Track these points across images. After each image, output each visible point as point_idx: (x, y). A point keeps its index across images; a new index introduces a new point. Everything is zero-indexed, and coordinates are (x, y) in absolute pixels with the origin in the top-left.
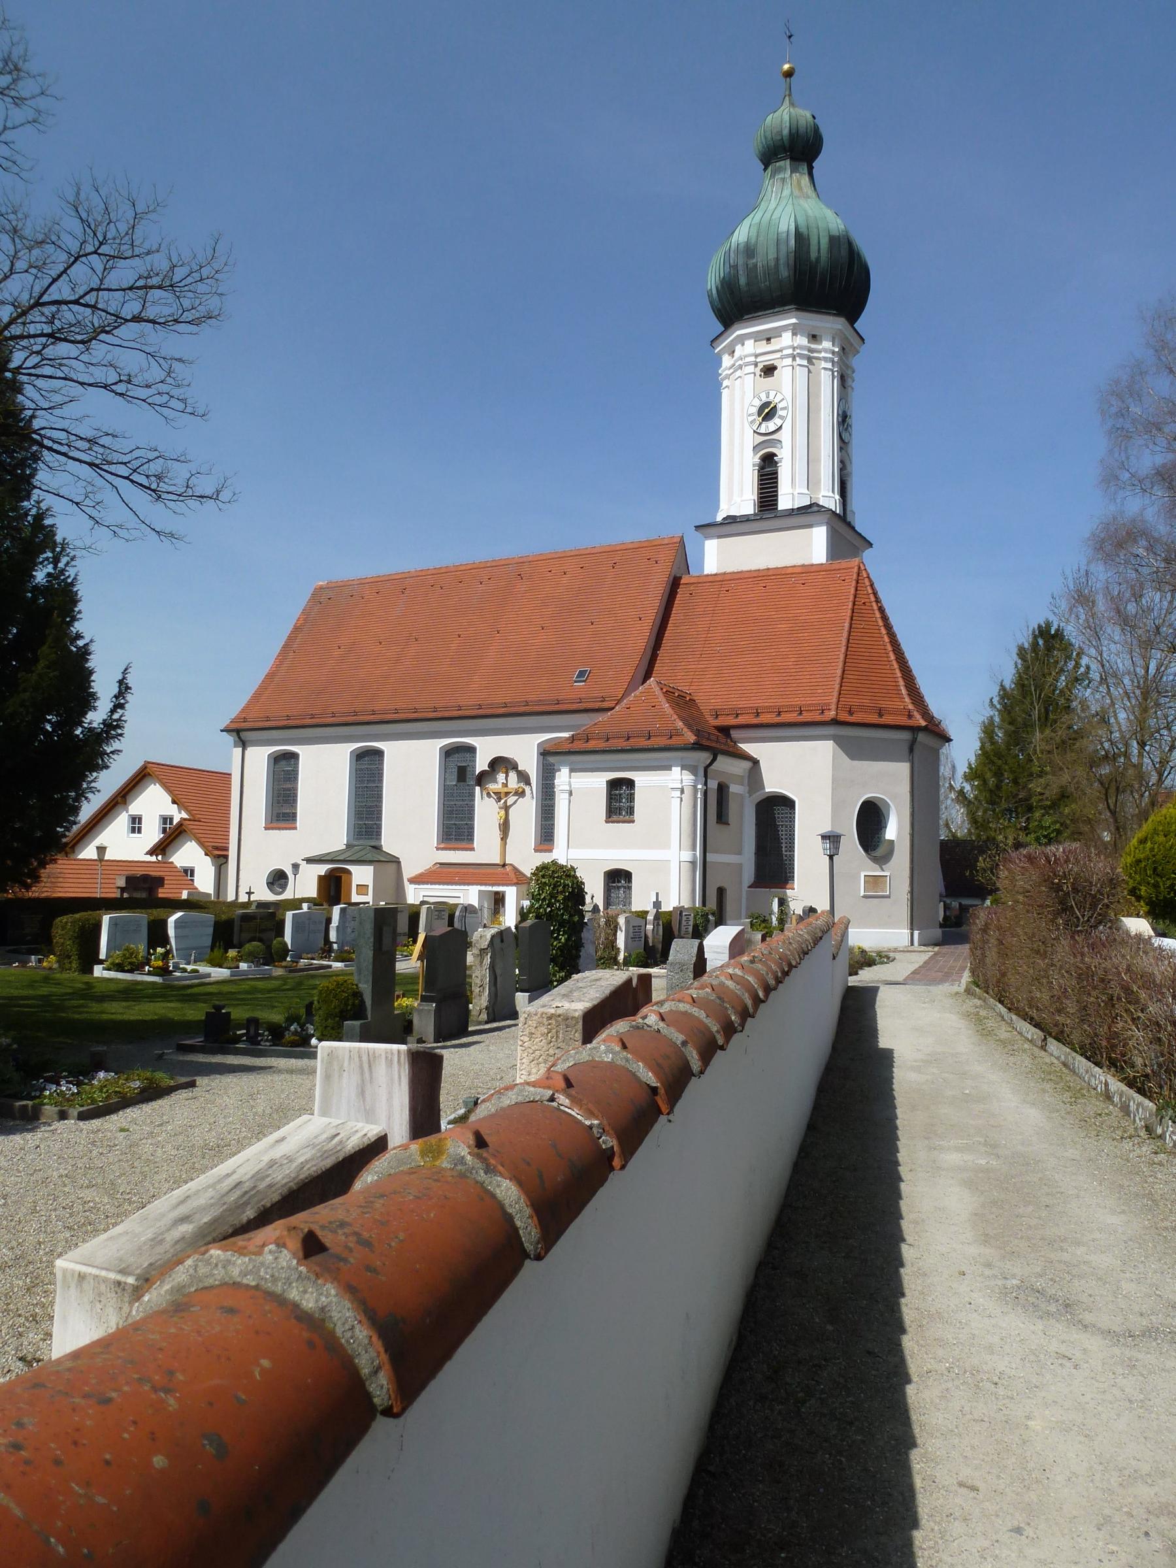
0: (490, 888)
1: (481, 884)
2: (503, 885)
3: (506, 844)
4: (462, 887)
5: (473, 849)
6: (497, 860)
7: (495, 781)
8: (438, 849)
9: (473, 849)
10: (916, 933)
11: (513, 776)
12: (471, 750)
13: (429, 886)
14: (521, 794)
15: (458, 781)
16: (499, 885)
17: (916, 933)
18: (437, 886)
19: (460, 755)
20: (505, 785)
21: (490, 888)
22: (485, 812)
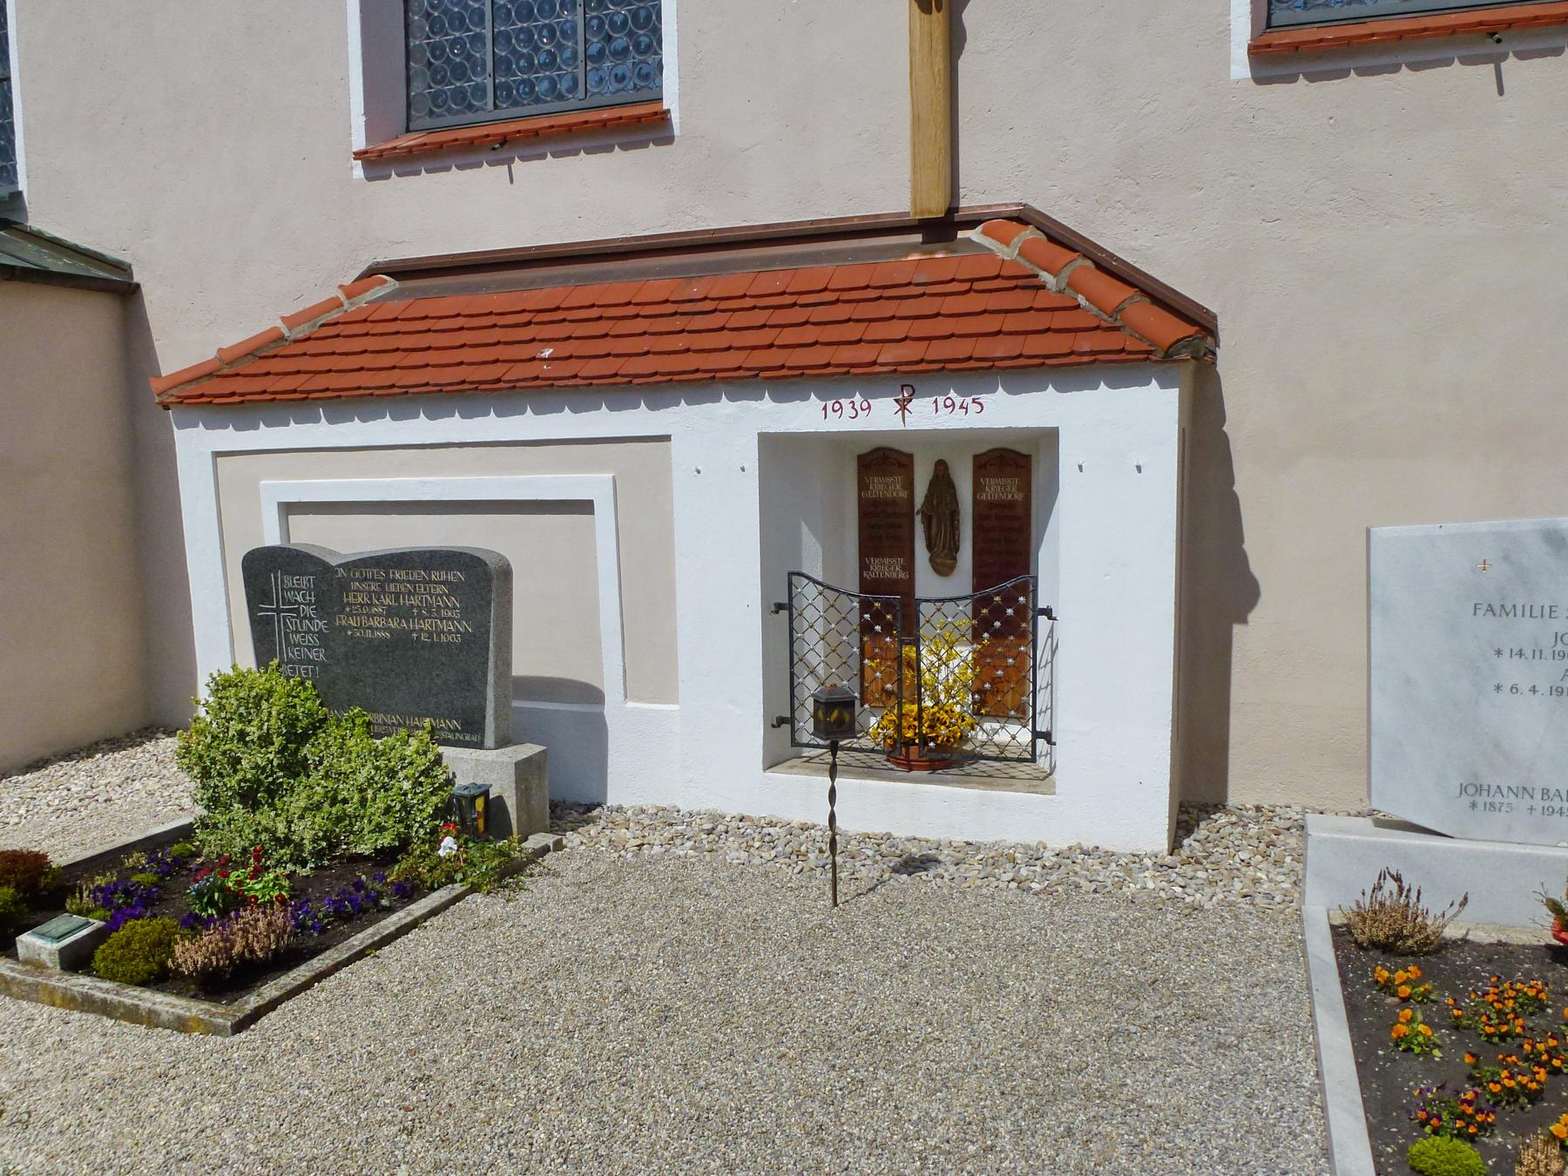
0: (1482, 526)
1: (787, 381)
2: (1025, 371)
3: (955, 40)
5: (649, 126)
6: (891, 193)
21: (1482, 526)
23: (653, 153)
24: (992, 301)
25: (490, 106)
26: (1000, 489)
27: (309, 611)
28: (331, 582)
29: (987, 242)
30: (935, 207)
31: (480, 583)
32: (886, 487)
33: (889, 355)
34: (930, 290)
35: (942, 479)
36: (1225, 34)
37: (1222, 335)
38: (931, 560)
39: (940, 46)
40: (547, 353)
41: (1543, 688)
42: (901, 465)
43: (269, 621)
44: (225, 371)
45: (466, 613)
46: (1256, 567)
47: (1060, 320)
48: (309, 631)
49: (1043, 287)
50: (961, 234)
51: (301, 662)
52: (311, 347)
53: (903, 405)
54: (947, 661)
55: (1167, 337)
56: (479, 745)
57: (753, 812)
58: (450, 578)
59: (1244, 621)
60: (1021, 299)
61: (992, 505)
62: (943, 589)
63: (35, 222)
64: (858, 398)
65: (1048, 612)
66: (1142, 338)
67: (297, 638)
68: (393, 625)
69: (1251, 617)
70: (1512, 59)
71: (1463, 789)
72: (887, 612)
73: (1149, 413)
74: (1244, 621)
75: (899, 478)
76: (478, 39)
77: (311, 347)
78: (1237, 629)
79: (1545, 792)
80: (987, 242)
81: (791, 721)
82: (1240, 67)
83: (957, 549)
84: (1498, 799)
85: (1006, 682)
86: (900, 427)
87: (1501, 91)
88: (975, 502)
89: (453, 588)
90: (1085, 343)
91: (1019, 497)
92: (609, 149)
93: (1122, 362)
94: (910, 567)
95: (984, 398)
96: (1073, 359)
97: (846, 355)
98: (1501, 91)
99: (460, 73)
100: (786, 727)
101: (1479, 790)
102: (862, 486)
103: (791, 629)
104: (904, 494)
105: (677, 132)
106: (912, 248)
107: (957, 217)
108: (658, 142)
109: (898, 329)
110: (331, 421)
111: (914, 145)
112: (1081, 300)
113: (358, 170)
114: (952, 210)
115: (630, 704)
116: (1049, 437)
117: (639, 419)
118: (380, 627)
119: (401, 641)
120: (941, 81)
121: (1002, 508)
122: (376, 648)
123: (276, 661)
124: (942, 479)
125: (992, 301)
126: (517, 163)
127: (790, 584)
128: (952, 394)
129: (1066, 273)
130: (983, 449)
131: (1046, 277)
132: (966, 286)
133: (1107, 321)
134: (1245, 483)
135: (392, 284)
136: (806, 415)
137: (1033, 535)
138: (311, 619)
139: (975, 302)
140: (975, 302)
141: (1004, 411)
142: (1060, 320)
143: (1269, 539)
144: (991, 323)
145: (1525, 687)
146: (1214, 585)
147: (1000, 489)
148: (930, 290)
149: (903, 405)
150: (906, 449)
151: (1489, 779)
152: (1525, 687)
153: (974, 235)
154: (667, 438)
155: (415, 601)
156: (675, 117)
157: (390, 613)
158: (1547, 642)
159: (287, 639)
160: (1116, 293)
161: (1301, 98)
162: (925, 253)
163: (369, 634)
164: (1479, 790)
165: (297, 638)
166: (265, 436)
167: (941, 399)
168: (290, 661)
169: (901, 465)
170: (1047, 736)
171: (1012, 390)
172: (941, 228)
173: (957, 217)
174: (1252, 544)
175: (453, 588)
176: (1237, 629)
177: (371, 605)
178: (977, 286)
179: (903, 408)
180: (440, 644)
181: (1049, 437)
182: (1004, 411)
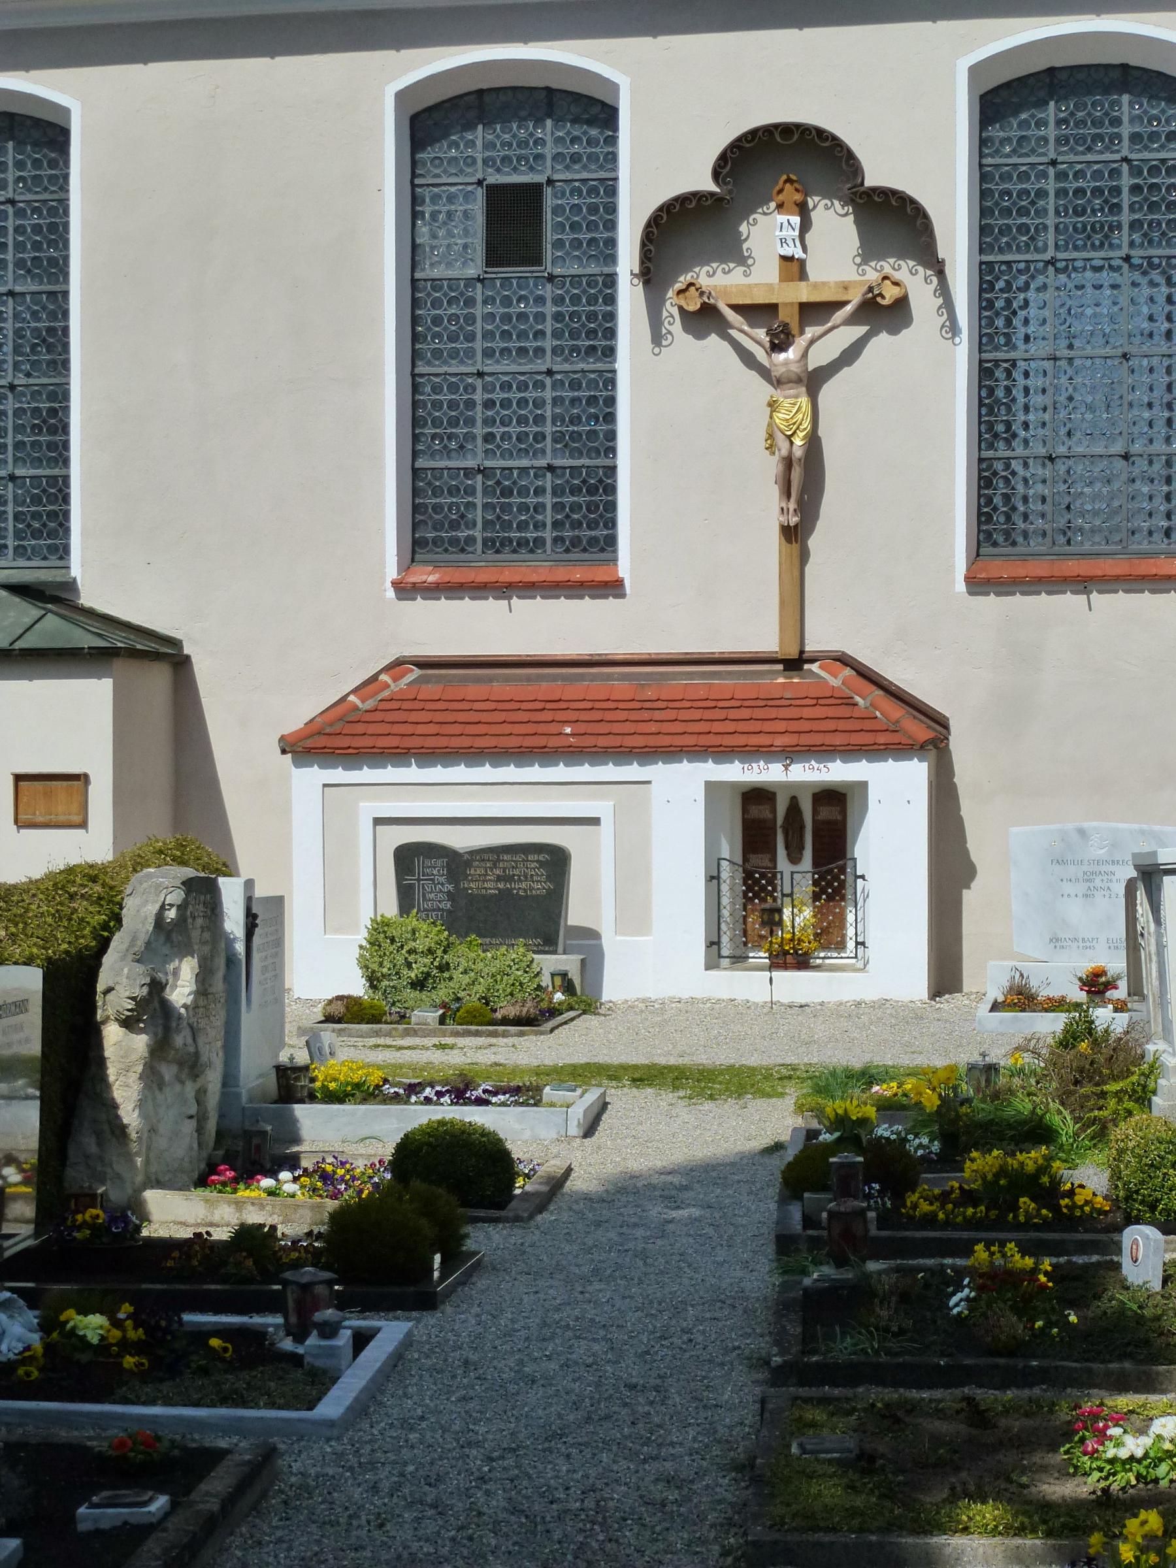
0: (1053, 827)
1: (723, 753)
2: (851, 752)
3: (804, 556)
4: (609, 771)
5: (613, 588)
6: (766, 638)
7: (733, 252)
8: (404, 590)
9: (613, 588)
10: (751, 955)
11: (835, 230)
12: (594, 111)
13: (412, 773)
14: (883, 313)
15: (494, 258)
16: (825, 752)
17: (751, 955)
18: (460, 772)
19: (499, 133)
20: (794, 268)
21: (1053, 827)
22: (677, 408)
23: (610, 604)
24: (830, 711)
25: (479, 551)
26: (826, 813)
27: (442, 879)
28: (456, 863)
29: (823, 674)
30: (793, 653)
31: (556, 861)
32: (760, 812)
33: (779, 741)
34: (793, 702)
35: (794, 807)
36: (951, 568)
37: (952, 729)
38: (788, 855)
39: (796, 561)
40: (568, 730)
41: (1080, 895)
42: (769, 799)
43: (411, 886)
44: (328, 731)
45: (549, 878)
46: (974, 857)
47: (868, 725)
48: (441, 891)
49: (856, 705)
50: (806, 666)
51: (434, 910)
52: (378, 716)
53: (786, 767)
54: (799, 917)
55: (920, 731)
56: (555, 952)
57: (699, 995)
58: (541, 858)
59: (969, 887)
60: (844, 711)
61: (824, 822)
62: (796, 875)
63: (87, 599)
64: (762, 763)
65: (863, 877)
66: (910, 737)
67: (432, 896)
68: (501, 886)
69: (973, 885)
70: (1095, 593)
71: (1051, 940)
72: (758, 888)
73: (913, 775)
74: (969, 887)
75: (767, 807)
76: (471, 506)
77: (378, 716)
78: (965, 892)
79: (1083, 939)
80: (823, 674)
81: (718, 943)
82: (961, 586)
83: (803, 848)
84: (1065, 944)
85: (830, 934)
86: (785, 779)
87: (1090, 609)
88: (814, 821)
89: (542, 864)
90: (882, 739)
91: (839, 818)
92: (582, 597)
93: (901, 749)
94: (774, 860)
95: (829, 765)
96: (876, 747)
97: (755, 740)
98: (1090, 609)
99: (455, 525)
100: (715, 947)
101: (1057, 940)
102: (745, 811)
103: (719, 890)
104: (770, 816)
105: (628, 591)
106: (777, 672)
107: (805, 656)
108: (616, 596)
109: (781, 726)
110: (419, 767)
111: (781, 616)
112: (878, 714)
113: (391, 593)
114: (802, 652)
115: (618, 938)
116: (863, 786)
117: (633, 771)
118: (491, 888)
119: (505, 894)
120: (798, 589)
121: (825, 830)
122: (487, 899)
123: (415, 910)
124: (794, 807)
125: (830, 711)
126: (515, 600)
127: (719, 864)
128: (813, 762)
129: (869, 698)
130: (745, 790)
131: (858, 699)
132: (814, 702)
133: (892, 727)
134: (968, 809)
135: (417, 672)
136: (736, 772)
137: (848, 841)
138: (442, 884)
139: (819, 712)
140: (819, 712)
141: (837, 772)
142: (868, 725)
143: (978, 845)
144: (831, 725)
145: (1073, 895)
146: (950, 868)
147: (826, 813)
148: (793, 702)
149: (786, 767)
150: (772, 790)
151: (1061, 935)
152: (1073, 895)
153: (814, 667)
154: (649, 782)
155: (516, 872)
156: (627, 583)
157: (499, 879)
158: (1080, 875)
159: (424, 895)
160: (896, 711)
161: (991, 603)
162: (786, 678)
163: (484, 891)
164: (1057, 940)
165: (432, 896)
166: (366, 774)
167: (807, 765)
168: (425, 910)
169: (769, 799)
170: (863, 944)
171: (844, 762)
172: (795, 664)
173: (805, 656)
174: (970, 845)
175: (542, 864)
176: (965, 892)
177: (487, 875)
178: (821, 702)
179: (786, 769)
180: (532, 896)
181: (863, 786)
182: (837, 772)
